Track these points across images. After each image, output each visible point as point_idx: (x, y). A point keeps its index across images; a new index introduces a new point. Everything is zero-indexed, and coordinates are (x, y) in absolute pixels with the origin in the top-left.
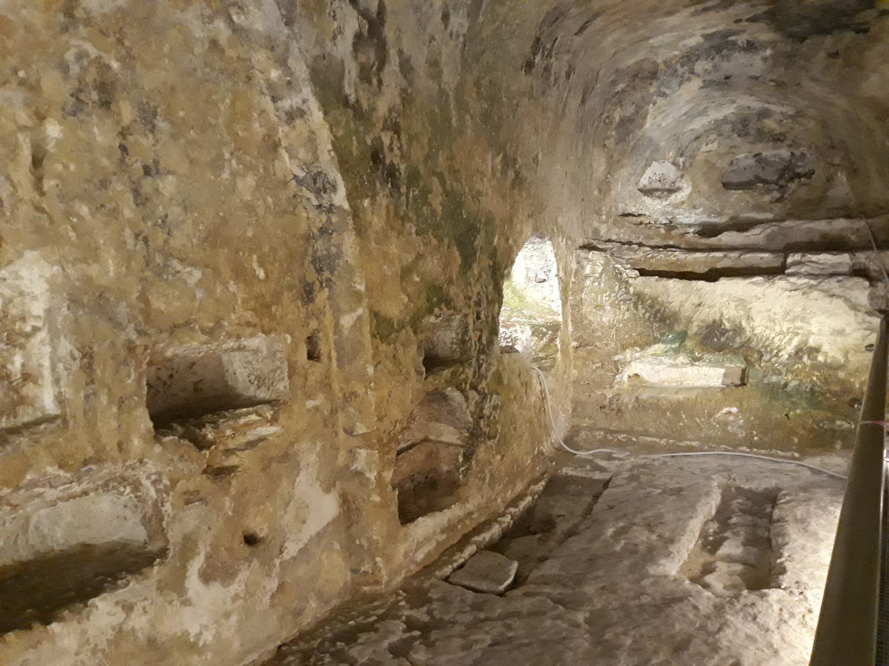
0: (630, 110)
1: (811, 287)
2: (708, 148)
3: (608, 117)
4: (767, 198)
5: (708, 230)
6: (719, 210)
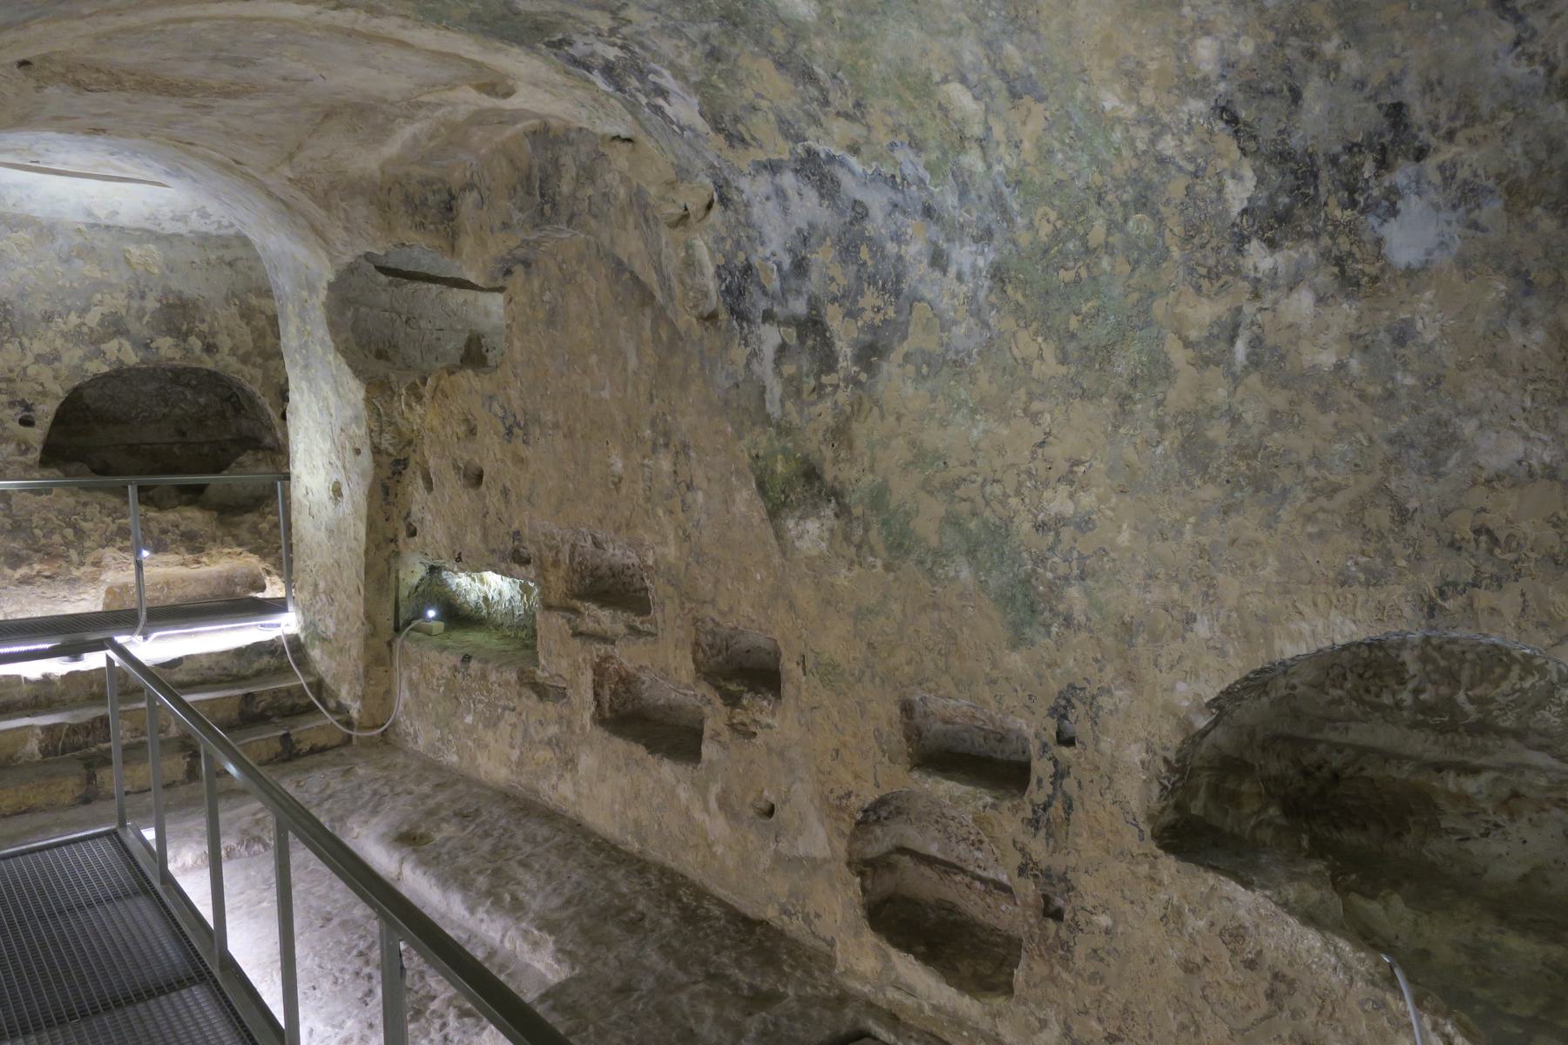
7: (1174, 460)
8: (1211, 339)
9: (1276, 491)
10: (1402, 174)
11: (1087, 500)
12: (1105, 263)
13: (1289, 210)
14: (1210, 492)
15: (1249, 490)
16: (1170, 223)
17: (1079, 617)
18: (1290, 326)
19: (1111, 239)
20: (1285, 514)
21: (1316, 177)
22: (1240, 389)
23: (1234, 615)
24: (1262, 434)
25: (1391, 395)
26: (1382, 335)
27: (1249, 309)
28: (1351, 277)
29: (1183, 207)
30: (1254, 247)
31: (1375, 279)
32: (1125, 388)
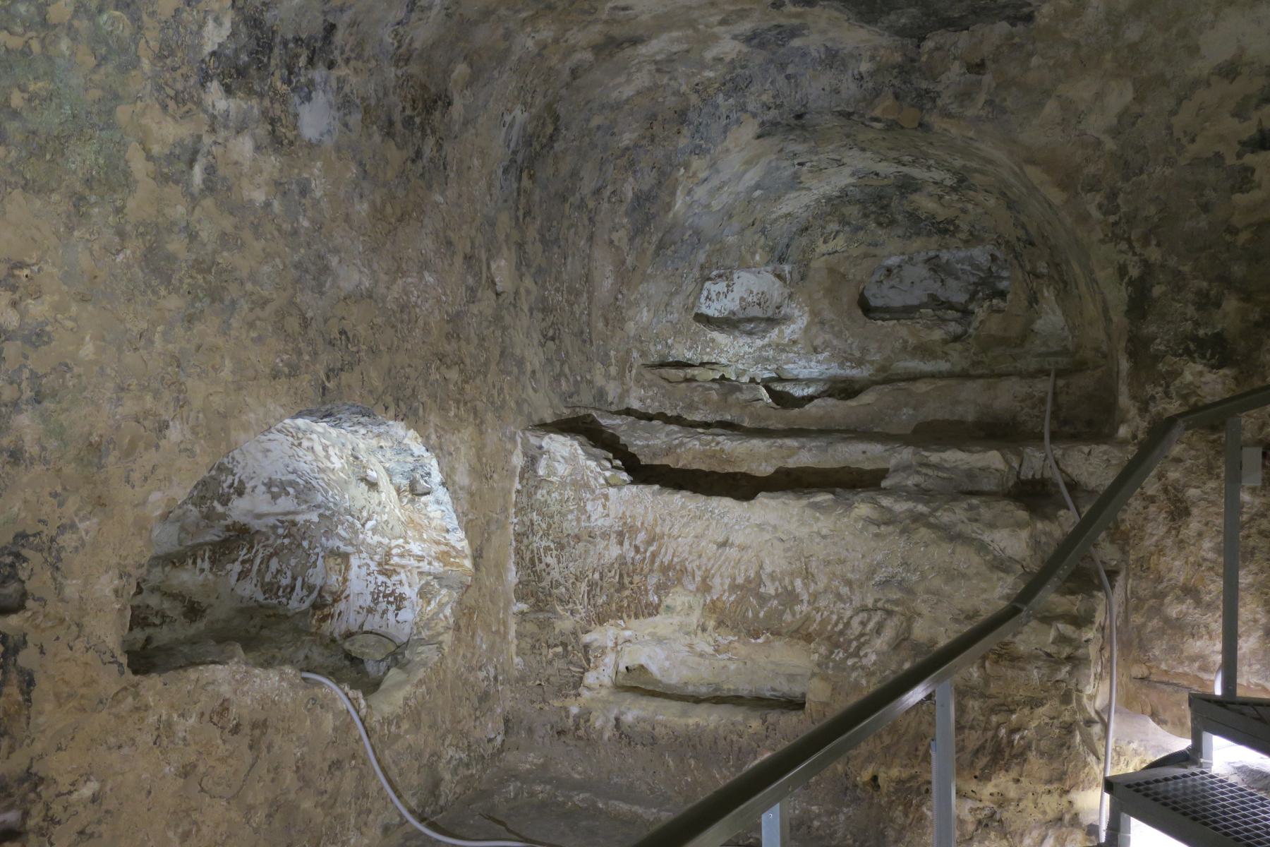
0: (648, 180)
1: (917, 518)
2: (831, 246)
3: (614, 192)
4: (937, 335)
5: (844, 390)
6: (858, 354)
7: (136, 269)
8: (171, 158)
9: (227, 302)
10: (319, 74)
11: (38, 309)
12: (64, 45)
13: (247, 66)
14: (173, 303)
15: (207, 300)
16: (149, 35)
17: (31, 449)
18: (236, 163)
19: (76, 23)
20: (235, 323)
21: (271, 50)
22: (198, 211)
23: (201, 415)
24: (215, 252)
25: (295, 232)
26: (294, 187)
27: (207, 139)
28: (279, 138)
29: (165, 25)
30: (214, 86)
31: (291, 143)
32: (78, 187)
